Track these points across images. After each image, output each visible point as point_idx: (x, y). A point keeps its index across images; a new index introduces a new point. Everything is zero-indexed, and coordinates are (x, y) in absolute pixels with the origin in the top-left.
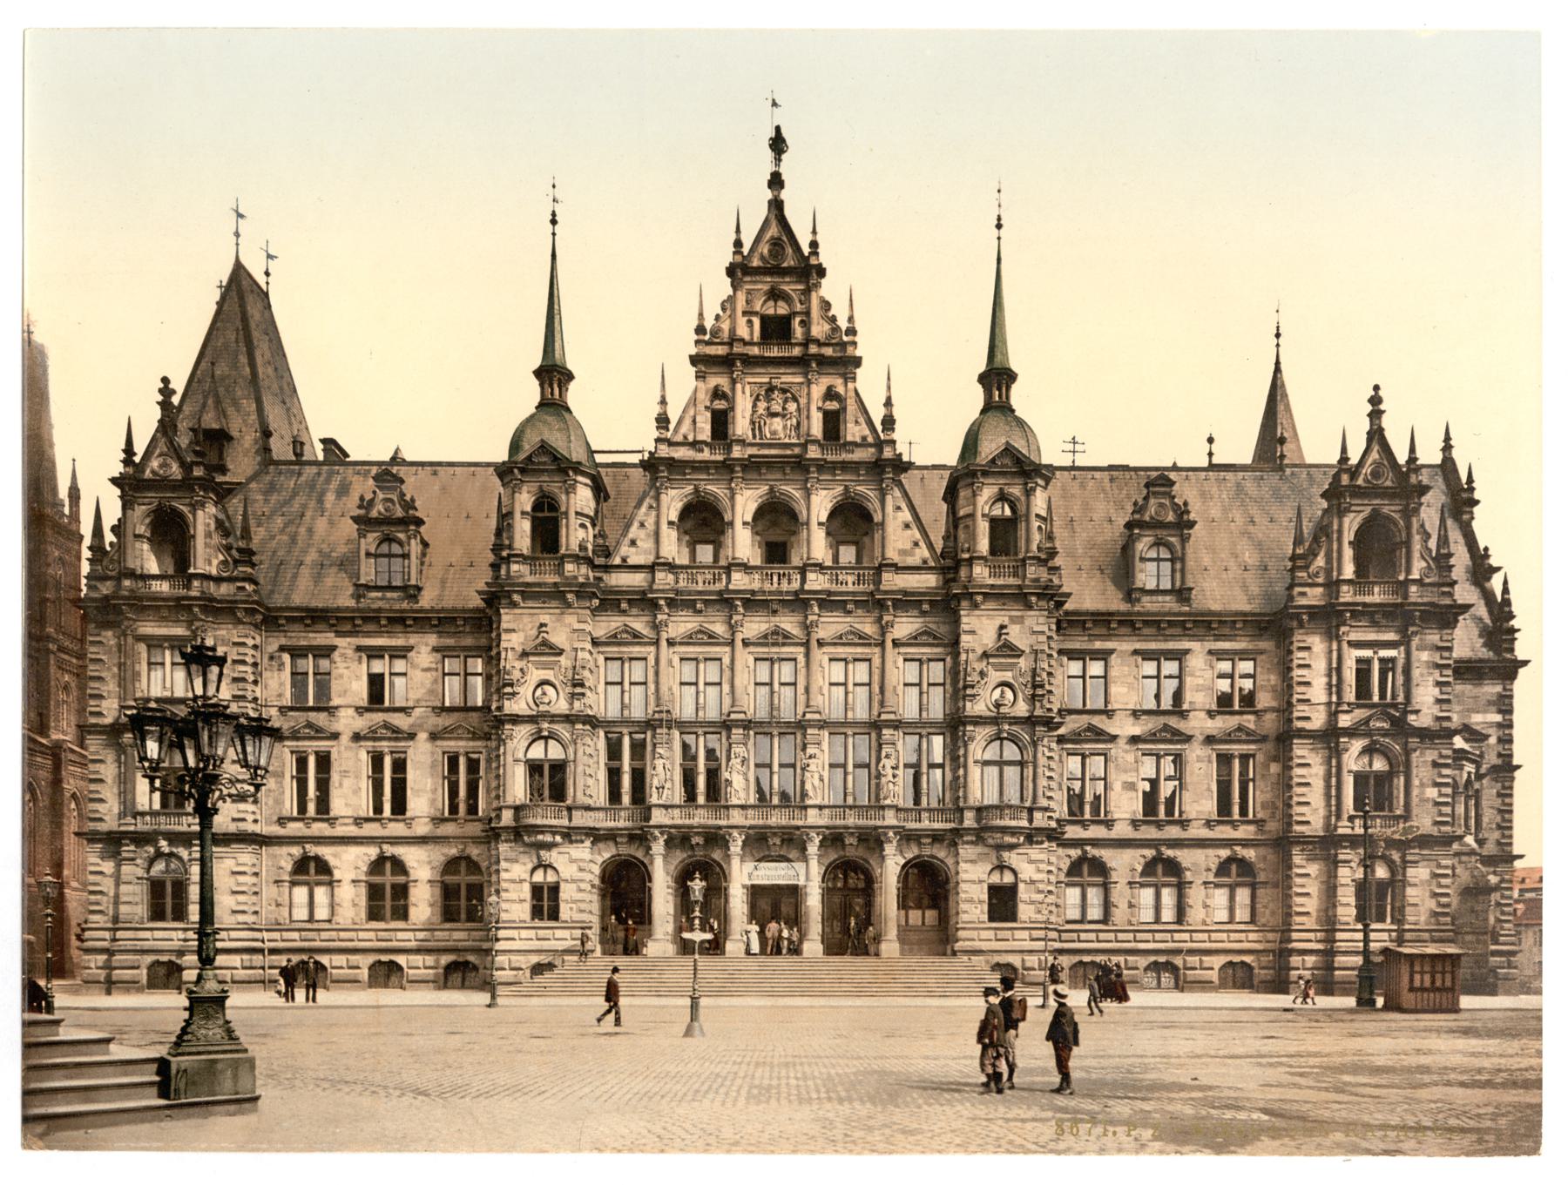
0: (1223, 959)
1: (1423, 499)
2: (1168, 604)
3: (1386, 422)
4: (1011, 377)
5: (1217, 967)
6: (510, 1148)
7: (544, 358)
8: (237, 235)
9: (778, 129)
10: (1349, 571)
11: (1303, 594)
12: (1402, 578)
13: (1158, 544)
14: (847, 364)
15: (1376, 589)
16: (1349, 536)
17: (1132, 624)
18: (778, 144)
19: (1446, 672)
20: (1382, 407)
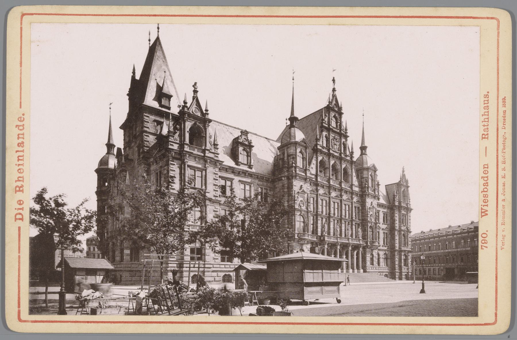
0: (223, 274)
1: (210, 124)
2: (246, 168)
3: (199, 95)
4: (366, 147)
5: (222, 276)
6: (30, 277)
7: (291, 115)
8: (158, 28)
9: (334, 78)
10: (187, 141)
11: (173, 145)
12: (203, 148)
13: (244, 150)
14: (346, 137)
15: (196, 150)
16: (187, 129)
17: (245, 173)
18: (334, 80)
19: (217, 187)
20: (197, 90)
